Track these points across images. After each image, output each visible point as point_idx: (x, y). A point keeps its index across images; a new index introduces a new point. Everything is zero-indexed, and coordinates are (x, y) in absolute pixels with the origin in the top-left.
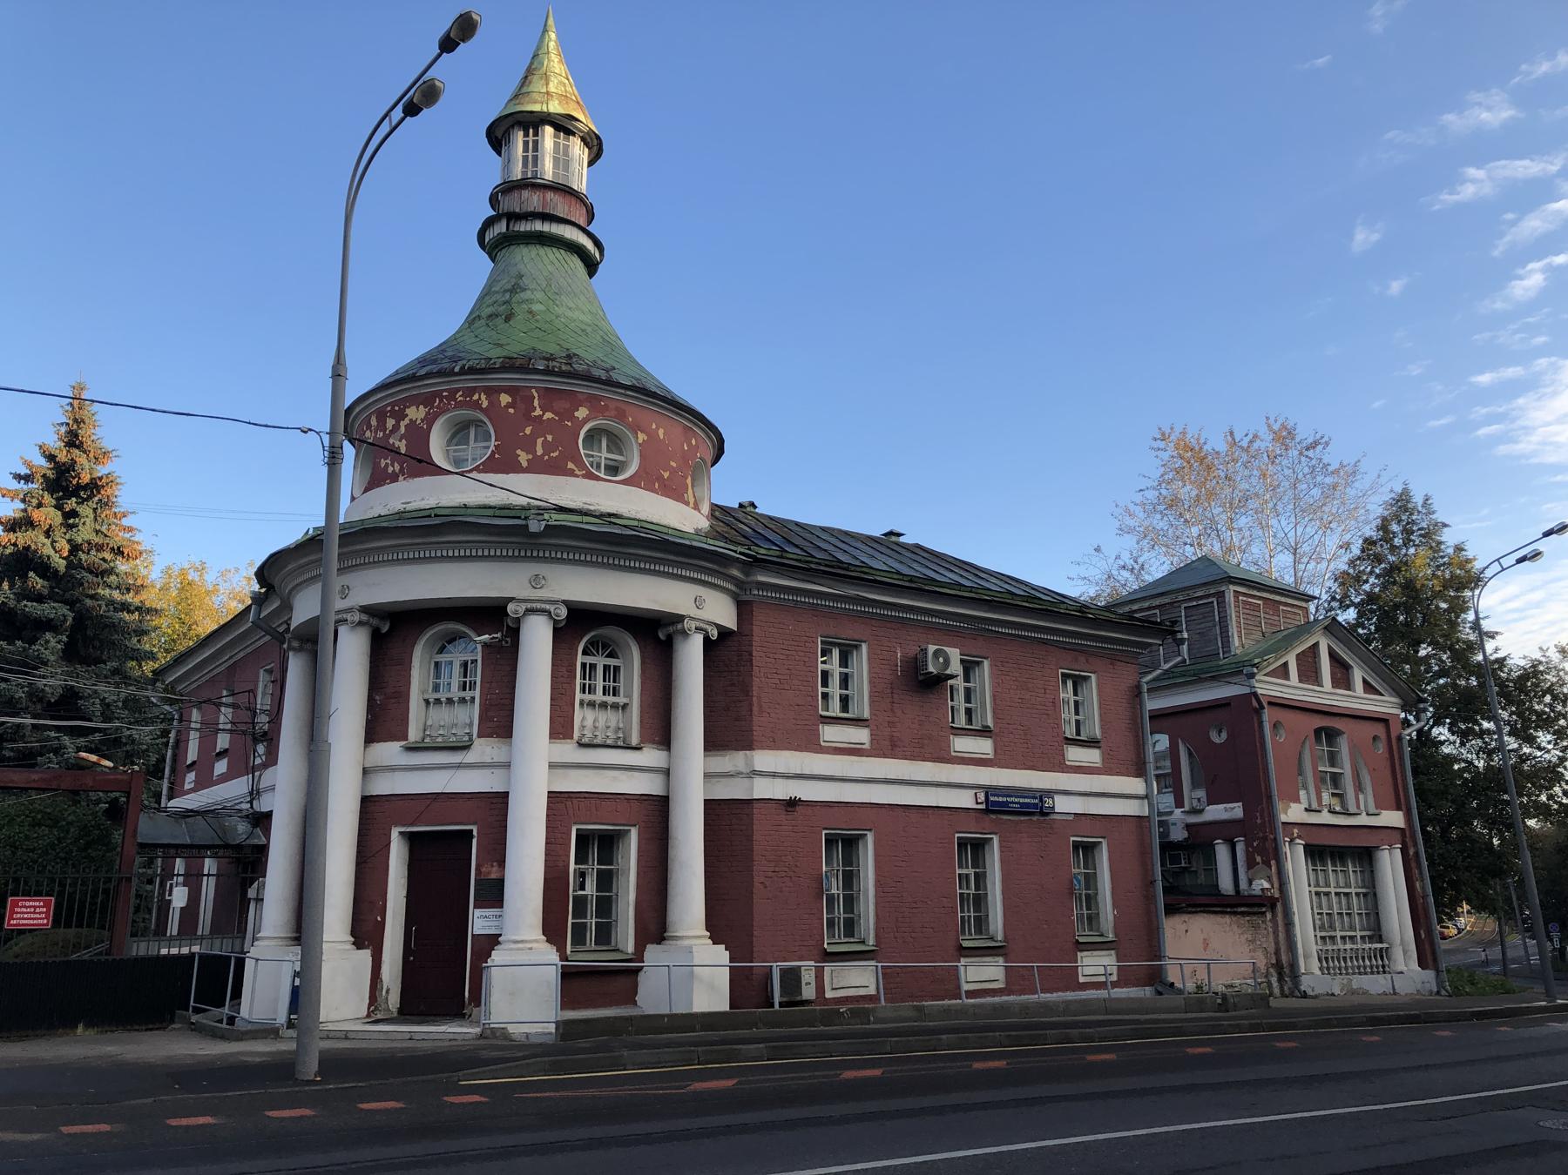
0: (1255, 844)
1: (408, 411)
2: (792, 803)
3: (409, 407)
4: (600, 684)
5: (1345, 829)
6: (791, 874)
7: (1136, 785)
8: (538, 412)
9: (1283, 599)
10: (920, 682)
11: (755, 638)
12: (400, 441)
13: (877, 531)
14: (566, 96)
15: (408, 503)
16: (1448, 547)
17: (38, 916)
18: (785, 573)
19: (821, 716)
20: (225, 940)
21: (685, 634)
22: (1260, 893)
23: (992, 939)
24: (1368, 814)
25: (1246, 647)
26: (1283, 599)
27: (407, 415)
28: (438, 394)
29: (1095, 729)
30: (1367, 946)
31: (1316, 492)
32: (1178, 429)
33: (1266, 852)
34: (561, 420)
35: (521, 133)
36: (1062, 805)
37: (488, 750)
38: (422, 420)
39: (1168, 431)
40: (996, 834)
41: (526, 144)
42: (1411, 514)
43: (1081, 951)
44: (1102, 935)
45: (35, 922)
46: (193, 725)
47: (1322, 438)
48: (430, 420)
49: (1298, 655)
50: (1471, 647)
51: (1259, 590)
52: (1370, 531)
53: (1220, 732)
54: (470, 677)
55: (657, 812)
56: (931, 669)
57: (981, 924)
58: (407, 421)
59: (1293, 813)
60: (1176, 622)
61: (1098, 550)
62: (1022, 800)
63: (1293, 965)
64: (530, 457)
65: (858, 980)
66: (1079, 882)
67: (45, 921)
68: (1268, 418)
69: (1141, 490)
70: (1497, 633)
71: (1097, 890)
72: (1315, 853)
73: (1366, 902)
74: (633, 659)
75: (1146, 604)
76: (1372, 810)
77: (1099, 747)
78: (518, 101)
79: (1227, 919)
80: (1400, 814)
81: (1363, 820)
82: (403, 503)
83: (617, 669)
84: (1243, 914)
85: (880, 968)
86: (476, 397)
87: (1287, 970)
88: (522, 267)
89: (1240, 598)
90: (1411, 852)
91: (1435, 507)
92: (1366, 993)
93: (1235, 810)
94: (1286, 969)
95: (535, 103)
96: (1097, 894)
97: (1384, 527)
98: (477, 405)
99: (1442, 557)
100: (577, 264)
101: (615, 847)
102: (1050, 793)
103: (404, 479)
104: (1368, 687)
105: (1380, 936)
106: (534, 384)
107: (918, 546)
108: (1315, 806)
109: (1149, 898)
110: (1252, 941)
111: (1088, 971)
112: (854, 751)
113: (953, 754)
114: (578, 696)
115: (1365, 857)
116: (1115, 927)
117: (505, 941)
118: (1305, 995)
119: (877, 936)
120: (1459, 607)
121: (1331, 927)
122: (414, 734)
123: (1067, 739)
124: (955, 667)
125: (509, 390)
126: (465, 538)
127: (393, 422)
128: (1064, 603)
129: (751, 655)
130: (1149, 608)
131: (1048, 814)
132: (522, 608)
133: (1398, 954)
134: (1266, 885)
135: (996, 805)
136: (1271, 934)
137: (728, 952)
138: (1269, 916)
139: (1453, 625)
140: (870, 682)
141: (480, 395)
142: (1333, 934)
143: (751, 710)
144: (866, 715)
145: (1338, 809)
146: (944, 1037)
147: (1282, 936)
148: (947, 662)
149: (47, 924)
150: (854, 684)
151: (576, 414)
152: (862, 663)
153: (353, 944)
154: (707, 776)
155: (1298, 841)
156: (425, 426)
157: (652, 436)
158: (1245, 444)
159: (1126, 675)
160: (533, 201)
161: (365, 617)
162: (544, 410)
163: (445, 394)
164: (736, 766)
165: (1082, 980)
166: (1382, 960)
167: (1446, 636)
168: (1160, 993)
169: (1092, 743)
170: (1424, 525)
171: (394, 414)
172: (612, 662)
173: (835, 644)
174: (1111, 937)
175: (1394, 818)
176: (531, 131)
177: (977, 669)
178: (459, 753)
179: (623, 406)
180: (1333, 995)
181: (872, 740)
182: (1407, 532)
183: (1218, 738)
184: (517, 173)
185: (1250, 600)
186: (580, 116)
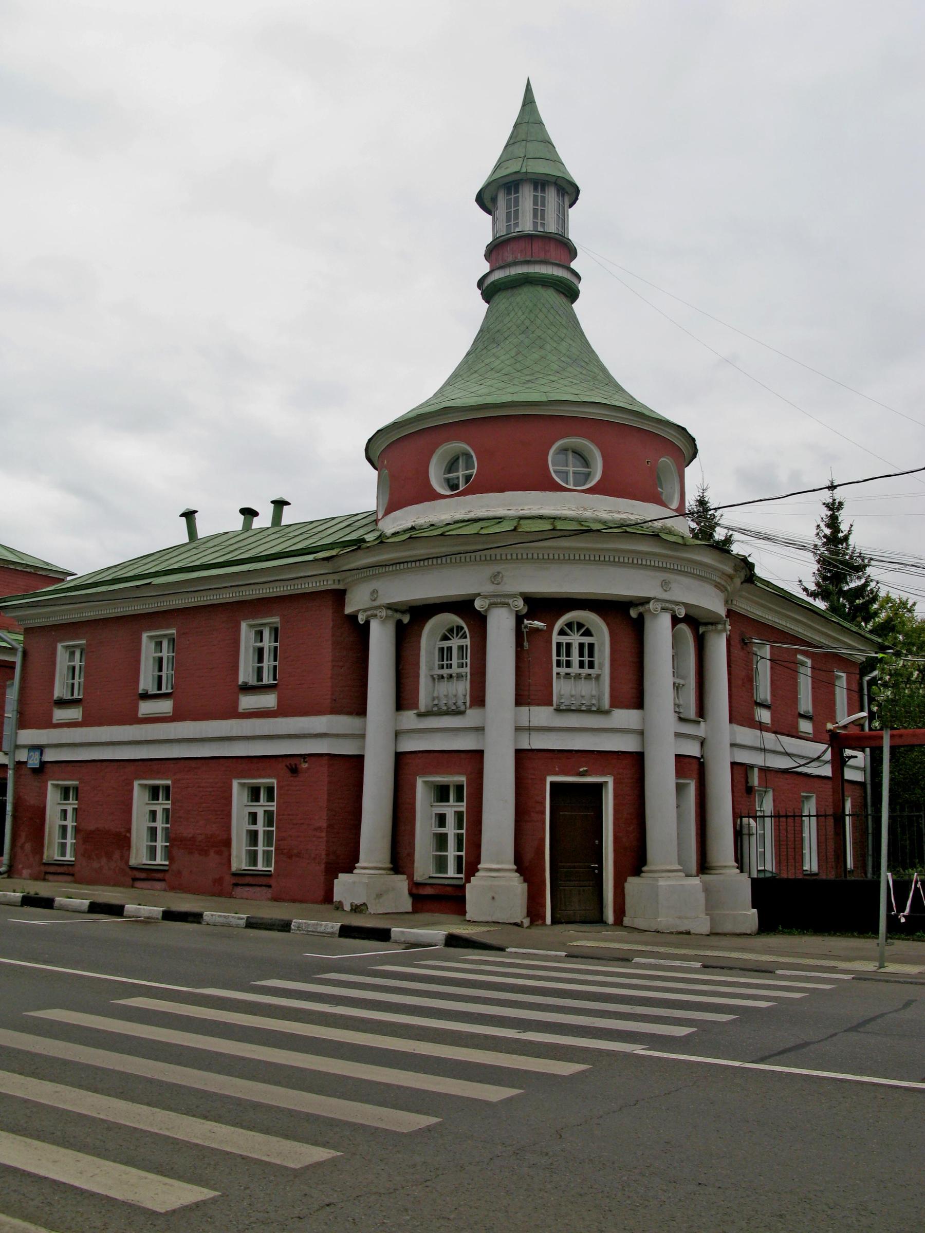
4: (575, 658)
54: (447, 661)
100: (551, 296)
114: (555, 670)
122: (423, 707)
132: (486, 603)
161: (390, 613)
172: (586, 640)
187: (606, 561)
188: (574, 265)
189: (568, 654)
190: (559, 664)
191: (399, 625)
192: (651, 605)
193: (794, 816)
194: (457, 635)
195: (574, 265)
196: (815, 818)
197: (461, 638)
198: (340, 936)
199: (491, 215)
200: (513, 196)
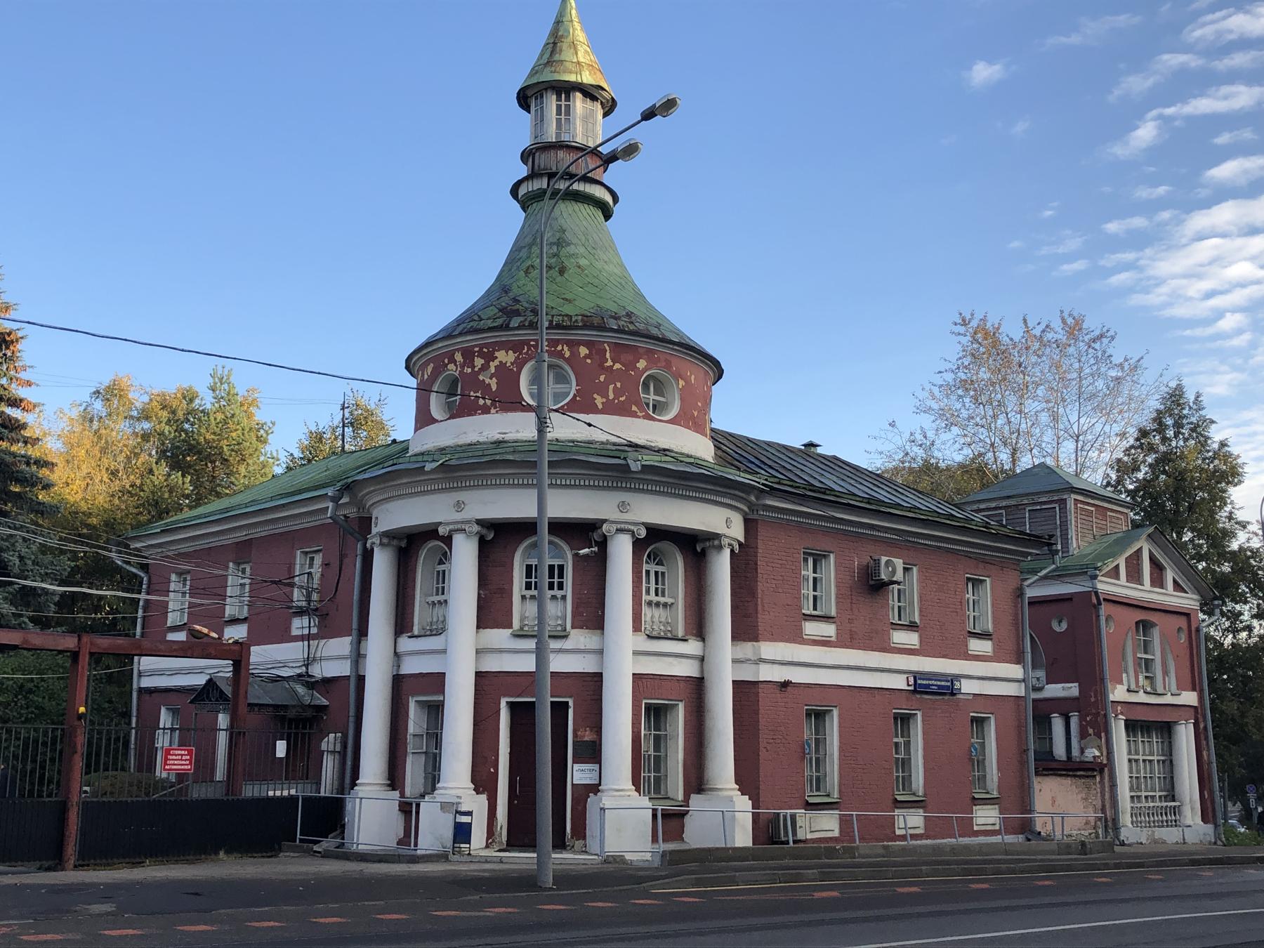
0: (1088, 719)
1: (497, 354)
2: (786, 685)
3: (498, 351)
5: (1156, 707)
6: (784, 741)
7: (1016, 671)
8: (609, 363)
9: (1110, 506)
10: (871, 586)
11: (760, 551)
12: (491, 378)
13: (797, 443)
14: (592, 66)
15: (505, 433)
16: (1214, 442)
17: (184, 762)
18: (788, 498)
19: (804, 614)
20: (255, 786)
22: (1092, 760)
23: (914, 794)
24: (1172, 695)
25: (1082, 548)
26: (1110, 506)
27: (496, 358)
28: (527, 343)
30: (1164, 804)
31: (1100, 384)
32: (978, 316)
33: (1097, 725)
34: (627, 370)
35: (554, 97)
36: (967, 687)
37: (582, 639)
38: (512, 364)
39: (968, 317)
40: (919, 710)
41: (559, 107)
42: (1183, 409)
43: (975, 805)
44: (988, 793)
45: (183, 767)
46: (228, 600)
47: (1108, 331)
48: (520, 364)
49: (1126, 559)
50: (1228, 534)
51: (1093, 498)
52: (1145, 419)
53: (1060, 622)
55: (697, 689)
56: (883, 577)
57: (907, 782)
58: (496, 362)
59: (1118, 693)
60: (1053, 536)
61: (892, 424)
62: (939, 683)
63: (1115, 821)
64: (604, 400)
65: (826, 825)
66: (976, 750)
67: (189, 767)
68: (1062, 312)
69: (940, 372)
70: (1248, 523)
71: (985, 755)
72: (1132, 727)
73: (1164, 767)
74: (678, 567)
75: (993, 505)
76: (1174, 689)
77: (991, 639)
78: (553, 69)
79: (1068, 781)
80: (1195, 694)
81: (1168, 699)
82: (500, 433)
83: (663, 574)
84: (1080, 777)
86: (559, 348)
87: (1110, 824)
88: (563, 221)
89: (1079, 505)
90: (1202, 726)
91: (1205, 403)
92: (1164, 842)
93: (1072, 690)
94: (1112, 824)
95: (570, 73)
96: (984, 759)
97: (1158, 419)
98: (560, 355)
99: (1208, 451)
100: (599, 214)
101: (662, 717)
102: (958, 677)
103: (497, 412)
104: (1177, 586)
105: (1173, 796)
106: (607, 339)
107: (835, 458)
108: (1133, 687)
109: (1023, 763)
110: (1086, 799)
111: (980, 821)
113: (892, 645)
115: (1166, 730)
116: (999, 787)
117: (606, 790)
118: (1123, 844)
119: (840, 791)
120: (1219, 498)
121: (1137, 788)
123: (969, 632)
125: (588, 344)
126: (578, 472)
127: (482, 361)
128: (974, 520)
129: (757, 564)
130: (995, 508)
131: (955, 694)
133: (1187, 811)
134: (1097, 754)
135: (922, 687)
136: (1099, 795)
138: (1098, 779)
139: (1212, 513)
140: (837, 586)
141: (563, 346)
142: (1139, 794)
143: (757, 610)
144: (833, 613)
145: (1149, 689)
146: (923, 868)
147: (1107, 796)
148: (894, 572)
149: (190, 770)
150: (823, 585)
151: (638, 365)
152: (830, 569)
154: (735, 661)
155: (1121, 717)
156: (515, 369)
157: (687, 381)
158: (1037, 332)
159: (1012, 579)
160: (565, 158)
162: (614, 362)
163: (532, 343)
164: (746, 654)
165: (976, 828)
166: (1175, 815)
167: (1206, 526)
168: (1029, 840)
170: (1194, 420)
171: (481, 355)
172: (660, 569)
173: (810, 554)
174: (995, 794)
175: (1190, 698)
176: (563, 95)
178: (559, 640)
179: (668, 357)
180: (1141, 843)
182: (1178, 425)
183: (1060, 627)
184: (551, 135)
185: (1086, 507)
186: (605, 86)
189: (561, 575)
190: (551, 587)
194: (654, 560)
196: (225, 732)
197: (657, 564)
200: (563, 103)
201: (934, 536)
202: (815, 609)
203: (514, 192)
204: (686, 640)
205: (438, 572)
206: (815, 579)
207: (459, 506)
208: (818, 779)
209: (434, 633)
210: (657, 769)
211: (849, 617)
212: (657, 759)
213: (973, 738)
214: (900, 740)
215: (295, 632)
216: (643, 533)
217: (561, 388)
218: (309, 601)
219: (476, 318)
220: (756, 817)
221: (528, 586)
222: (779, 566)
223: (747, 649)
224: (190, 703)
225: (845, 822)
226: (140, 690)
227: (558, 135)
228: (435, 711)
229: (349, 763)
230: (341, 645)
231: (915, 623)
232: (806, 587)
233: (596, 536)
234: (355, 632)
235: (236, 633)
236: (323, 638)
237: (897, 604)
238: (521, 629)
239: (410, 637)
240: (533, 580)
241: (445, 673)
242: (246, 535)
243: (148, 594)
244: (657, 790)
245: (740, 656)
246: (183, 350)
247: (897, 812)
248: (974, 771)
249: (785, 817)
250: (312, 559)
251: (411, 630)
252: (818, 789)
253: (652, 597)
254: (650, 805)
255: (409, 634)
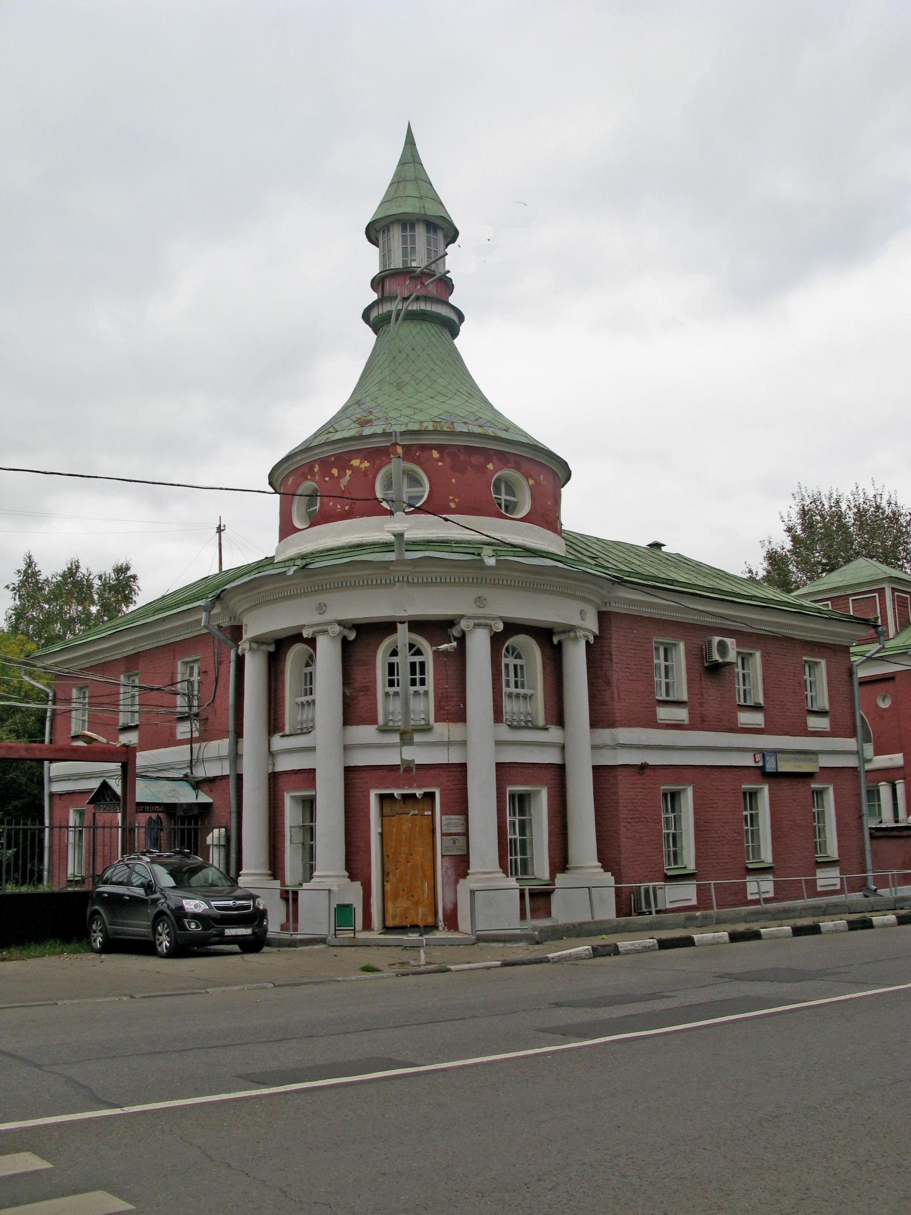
11: (614, 641)
21: (576, 639)
29: (823, 702)
46: (121, 708)
83: (522, 667)
85: (845, 880)
93: (897, 759)
96: (825, 826)
112: (678, 726)
113: (739, 726)
124: (732, 656)
129: (611, 654)
137: (613, 877)
143: (613, 697)
153: (348, 877)
165: (819, 889)
169: (756, 708)
172: (518, 662)
177: (750, 660)
181: (690, 717)
183: (884, 705)
184: (397, 263)
187: (456, 583)
188: (452, 300)
189: (423, 672)
190: (413, 683)
191: (345, 642)
192: (463, 624)
193: (111, 828)
194: (513, 653)
195: (452, 300)
197: (515, 658)
198: (851, 929)
199: (378, 246)
200: (408, 234)
201: (772, 622)
202: (667, 695)
203: (366, 316)
204: (546, 729)
205: (306, 674)
206: (666, 667)
207: (321, 609)
208: (675, 853)
209: (305, 731)
210: (523, 852)
211: (699, 701)
212: (523, 842)
213: (814, 807)
214: (747, 813)
215: (179, 737)
216: (500, 627)
217: (415, 490)
218: (190, 706)
219: (331, 430)
220: (618, 892)
221: (391, 683)
222: (631, 655)
223: (606, 735)
224: (88, 803)
225: (702, 892)
226: (52, 795)
227: (404, 262)
228: (309, 805)
229: (233, 855)
230: (222, 746)
231: (760, 704)
232: (658, 676)
233: (455, 632)
234: (232, 734)
235: (131, 738)
236: (204, 740)
237: (742, 688)
238: (386, 724)
239: (282, 736)
240: (396, 677)
241: (315, 769)
242: (133, 649)
243: (54, 704)
244: (525, 871)
245: (598, 742)
246: (45, 473)
247: (748, 878)
248: (816, 838)
249: (647, 891)
250: (192, 668)
251: (283, 729)
252: (676, 863)
253: (512, 689)
254: (517, 885)
255: (281, 734)
